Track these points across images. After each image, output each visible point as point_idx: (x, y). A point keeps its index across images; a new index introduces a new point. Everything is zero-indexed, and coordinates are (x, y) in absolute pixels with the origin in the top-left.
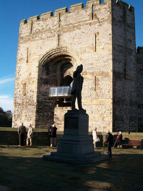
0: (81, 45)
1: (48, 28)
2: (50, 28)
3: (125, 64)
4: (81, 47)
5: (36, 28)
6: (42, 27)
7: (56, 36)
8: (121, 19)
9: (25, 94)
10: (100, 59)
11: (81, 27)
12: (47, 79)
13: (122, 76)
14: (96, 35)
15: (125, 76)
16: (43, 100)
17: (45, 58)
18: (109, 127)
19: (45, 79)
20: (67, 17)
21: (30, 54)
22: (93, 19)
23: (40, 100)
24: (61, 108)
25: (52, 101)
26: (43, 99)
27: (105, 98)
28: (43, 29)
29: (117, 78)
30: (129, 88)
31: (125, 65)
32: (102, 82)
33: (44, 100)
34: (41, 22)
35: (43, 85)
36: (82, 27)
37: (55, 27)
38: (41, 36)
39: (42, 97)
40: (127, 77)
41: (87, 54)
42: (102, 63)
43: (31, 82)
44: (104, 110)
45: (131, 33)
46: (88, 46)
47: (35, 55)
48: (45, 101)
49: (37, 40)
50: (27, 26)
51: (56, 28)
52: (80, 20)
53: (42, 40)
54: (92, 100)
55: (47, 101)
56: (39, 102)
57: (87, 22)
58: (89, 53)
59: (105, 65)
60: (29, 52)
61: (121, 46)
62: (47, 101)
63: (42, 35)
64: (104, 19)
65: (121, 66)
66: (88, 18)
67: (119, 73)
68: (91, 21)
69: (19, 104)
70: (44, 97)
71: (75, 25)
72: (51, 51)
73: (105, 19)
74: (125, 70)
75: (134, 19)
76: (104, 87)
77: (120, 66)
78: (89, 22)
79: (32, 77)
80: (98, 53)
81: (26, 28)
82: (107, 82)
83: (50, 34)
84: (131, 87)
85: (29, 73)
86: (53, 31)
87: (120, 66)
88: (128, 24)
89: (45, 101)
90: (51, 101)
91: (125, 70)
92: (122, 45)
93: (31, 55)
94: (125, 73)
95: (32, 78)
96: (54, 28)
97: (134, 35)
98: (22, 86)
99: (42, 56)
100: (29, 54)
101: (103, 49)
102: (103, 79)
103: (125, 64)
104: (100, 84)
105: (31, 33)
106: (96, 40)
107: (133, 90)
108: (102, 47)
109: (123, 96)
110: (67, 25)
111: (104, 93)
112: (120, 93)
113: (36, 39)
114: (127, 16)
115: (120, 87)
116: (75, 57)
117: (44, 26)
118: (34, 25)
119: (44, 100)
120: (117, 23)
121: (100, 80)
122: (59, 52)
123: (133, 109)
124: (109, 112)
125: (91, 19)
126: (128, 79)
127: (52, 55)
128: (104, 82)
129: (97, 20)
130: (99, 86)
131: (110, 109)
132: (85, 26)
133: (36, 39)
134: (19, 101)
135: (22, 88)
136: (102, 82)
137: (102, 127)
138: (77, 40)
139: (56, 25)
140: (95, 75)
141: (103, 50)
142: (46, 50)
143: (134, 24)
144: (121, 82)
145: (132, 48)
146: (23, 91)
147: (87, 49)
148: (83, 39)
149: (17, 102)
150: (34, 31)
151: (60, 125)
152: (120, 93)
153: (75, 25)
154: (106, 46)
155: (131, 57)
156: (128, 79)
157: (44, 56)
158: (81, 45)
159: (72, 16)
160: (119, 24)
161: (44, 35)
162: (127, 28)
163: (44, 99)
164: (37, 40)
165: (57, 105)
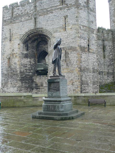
0: (53, 26)
1: (26, 12)
2: (28, 12)
3: (89, 40)
4: (54, 27)
5: (16, 12)
6: (22, 12)
7: (33, 19)
8: (85, 5)
9: (10, 66)
10: (69, 36)
11: (53, 12)
12: (27, 54)
13: (86, 50)
14: (65, 18)
15: (89, 50)
16: (24, 71)
17: (24, 37)
18: (77, 90)
19: (26, 54)
20: (42, 3)
21: (12, 34)
22: (62, 4)
23: (22, 71)
24: (39, 76)
25: (32, 71)
26: (24, 70)
27: (73, 67)
28: (22, 13)
29: (83, 52)
30: (92, 59)
31: (89, 41)
32: (71, 55)
33: (25, 71)
34: (20, 7)
35: (24, 59)
36: (54, 11)
37: (32, 12)
38: (21, 19)
39: (24, 68)
40: (90, 50)
41: (59, 33)
42: (71, 40)
43: (15, 56)
44: (73, 76)
45: (93, 16)
46: (59, 26)
47: (17, 34)
48: (26, 71)
49: (18, 22)
50: (9, 11)
51: (33, 12)
52: (53, 5)
53: (21, 22)
54: (64, 69)
55: (27, 71)
56: (22, 72)
57: (58, 7)
58: (60, 32)
59: (73, 41)
60: (11, 33)
61: (86, 26)
62: (27, 71)
63: (22, 18)
64: (71, 4)
65: (86, 42)
66: (59, 4)
67: (84, 47)
68: (61, 6)
69: (5, 74)
70: (25, 68)
71: (48, 10)
72: (29, 31)
73: (72, 4)
74: (88, 45)
75: (95, 4)
76: (72, 59)
77: (84, 42)
78: (59, 7)
79: (15, 52)
80: (67, 32)
81: (7, 13)
82: (75, 55)
83: (28, 17)
84: (94, 58)
85: (12, 50)
86: (30, 15)
87: (84, 42)
88: (91, 8)
89: (26, 71)
90: (31, 71)
91: (88, 45)
92: (86, 25)
93: (13, 35)
94: (89, 48)
95: (15, 54)
96: (31, 12)
97: (95, 18)
98: (7, 60)
99: (22, 36)
100: (11, 34)
101: (71, 28)
102: (72, 53)
103: (89, 40)
104: (70, 57)
105: (12, 17)
106: (65, 22)
107: (95, 61)
108: (70, 27)
109: (88, 65)
110: (41, 10)
111: (73, 64)
112: (85, 63)
113: (17, 21)
114: (90, 2)
115: (85, 58)
116: (49, 36)
117: (23, 11)
118: (14, 10)
119: (25, 71)
120: (82, 8)
121: (70, 53)
122: (36, 32)
123: (95, 75)
124: (77, 78)
125: (61, 5)
126: (91, 52)
127: (30, 35)
128: (73, 55)
129: (66, 5)
130: (69, 58)
131: (78, 76)
132: (56, 10)
133: (17, 21)
134: (5, 72)
135: (7, 61)
136: (71, 55)
137: (72, 90)
138: (50, 22)
139: (32, 10)
140: (65, 50)
141: (71, 30)
142: (26, 31)
143: (95, 8)
144: (86, 54)
145: (94, 28)
146: (8, 64)
147: (58, 29)
148: (55, 21)
149: (3, 73)
150: (15, 15)
151: (38, 90)
152: (85, 63)
153: (48, 10)
154: (74, 26)
155: (93, 35)
156: (91, 52)
157: (24, 36)
158: (53, 26)
159: (45, 2)
160: (83, 8)
161: (23, 18)
162: (90, 12)
163: (25, 70)
164: (18, 22)
165: (36, 74)
